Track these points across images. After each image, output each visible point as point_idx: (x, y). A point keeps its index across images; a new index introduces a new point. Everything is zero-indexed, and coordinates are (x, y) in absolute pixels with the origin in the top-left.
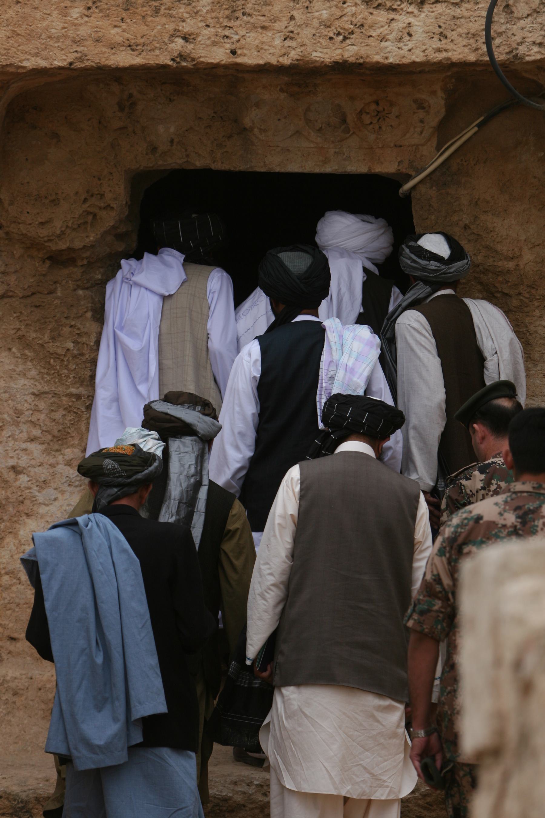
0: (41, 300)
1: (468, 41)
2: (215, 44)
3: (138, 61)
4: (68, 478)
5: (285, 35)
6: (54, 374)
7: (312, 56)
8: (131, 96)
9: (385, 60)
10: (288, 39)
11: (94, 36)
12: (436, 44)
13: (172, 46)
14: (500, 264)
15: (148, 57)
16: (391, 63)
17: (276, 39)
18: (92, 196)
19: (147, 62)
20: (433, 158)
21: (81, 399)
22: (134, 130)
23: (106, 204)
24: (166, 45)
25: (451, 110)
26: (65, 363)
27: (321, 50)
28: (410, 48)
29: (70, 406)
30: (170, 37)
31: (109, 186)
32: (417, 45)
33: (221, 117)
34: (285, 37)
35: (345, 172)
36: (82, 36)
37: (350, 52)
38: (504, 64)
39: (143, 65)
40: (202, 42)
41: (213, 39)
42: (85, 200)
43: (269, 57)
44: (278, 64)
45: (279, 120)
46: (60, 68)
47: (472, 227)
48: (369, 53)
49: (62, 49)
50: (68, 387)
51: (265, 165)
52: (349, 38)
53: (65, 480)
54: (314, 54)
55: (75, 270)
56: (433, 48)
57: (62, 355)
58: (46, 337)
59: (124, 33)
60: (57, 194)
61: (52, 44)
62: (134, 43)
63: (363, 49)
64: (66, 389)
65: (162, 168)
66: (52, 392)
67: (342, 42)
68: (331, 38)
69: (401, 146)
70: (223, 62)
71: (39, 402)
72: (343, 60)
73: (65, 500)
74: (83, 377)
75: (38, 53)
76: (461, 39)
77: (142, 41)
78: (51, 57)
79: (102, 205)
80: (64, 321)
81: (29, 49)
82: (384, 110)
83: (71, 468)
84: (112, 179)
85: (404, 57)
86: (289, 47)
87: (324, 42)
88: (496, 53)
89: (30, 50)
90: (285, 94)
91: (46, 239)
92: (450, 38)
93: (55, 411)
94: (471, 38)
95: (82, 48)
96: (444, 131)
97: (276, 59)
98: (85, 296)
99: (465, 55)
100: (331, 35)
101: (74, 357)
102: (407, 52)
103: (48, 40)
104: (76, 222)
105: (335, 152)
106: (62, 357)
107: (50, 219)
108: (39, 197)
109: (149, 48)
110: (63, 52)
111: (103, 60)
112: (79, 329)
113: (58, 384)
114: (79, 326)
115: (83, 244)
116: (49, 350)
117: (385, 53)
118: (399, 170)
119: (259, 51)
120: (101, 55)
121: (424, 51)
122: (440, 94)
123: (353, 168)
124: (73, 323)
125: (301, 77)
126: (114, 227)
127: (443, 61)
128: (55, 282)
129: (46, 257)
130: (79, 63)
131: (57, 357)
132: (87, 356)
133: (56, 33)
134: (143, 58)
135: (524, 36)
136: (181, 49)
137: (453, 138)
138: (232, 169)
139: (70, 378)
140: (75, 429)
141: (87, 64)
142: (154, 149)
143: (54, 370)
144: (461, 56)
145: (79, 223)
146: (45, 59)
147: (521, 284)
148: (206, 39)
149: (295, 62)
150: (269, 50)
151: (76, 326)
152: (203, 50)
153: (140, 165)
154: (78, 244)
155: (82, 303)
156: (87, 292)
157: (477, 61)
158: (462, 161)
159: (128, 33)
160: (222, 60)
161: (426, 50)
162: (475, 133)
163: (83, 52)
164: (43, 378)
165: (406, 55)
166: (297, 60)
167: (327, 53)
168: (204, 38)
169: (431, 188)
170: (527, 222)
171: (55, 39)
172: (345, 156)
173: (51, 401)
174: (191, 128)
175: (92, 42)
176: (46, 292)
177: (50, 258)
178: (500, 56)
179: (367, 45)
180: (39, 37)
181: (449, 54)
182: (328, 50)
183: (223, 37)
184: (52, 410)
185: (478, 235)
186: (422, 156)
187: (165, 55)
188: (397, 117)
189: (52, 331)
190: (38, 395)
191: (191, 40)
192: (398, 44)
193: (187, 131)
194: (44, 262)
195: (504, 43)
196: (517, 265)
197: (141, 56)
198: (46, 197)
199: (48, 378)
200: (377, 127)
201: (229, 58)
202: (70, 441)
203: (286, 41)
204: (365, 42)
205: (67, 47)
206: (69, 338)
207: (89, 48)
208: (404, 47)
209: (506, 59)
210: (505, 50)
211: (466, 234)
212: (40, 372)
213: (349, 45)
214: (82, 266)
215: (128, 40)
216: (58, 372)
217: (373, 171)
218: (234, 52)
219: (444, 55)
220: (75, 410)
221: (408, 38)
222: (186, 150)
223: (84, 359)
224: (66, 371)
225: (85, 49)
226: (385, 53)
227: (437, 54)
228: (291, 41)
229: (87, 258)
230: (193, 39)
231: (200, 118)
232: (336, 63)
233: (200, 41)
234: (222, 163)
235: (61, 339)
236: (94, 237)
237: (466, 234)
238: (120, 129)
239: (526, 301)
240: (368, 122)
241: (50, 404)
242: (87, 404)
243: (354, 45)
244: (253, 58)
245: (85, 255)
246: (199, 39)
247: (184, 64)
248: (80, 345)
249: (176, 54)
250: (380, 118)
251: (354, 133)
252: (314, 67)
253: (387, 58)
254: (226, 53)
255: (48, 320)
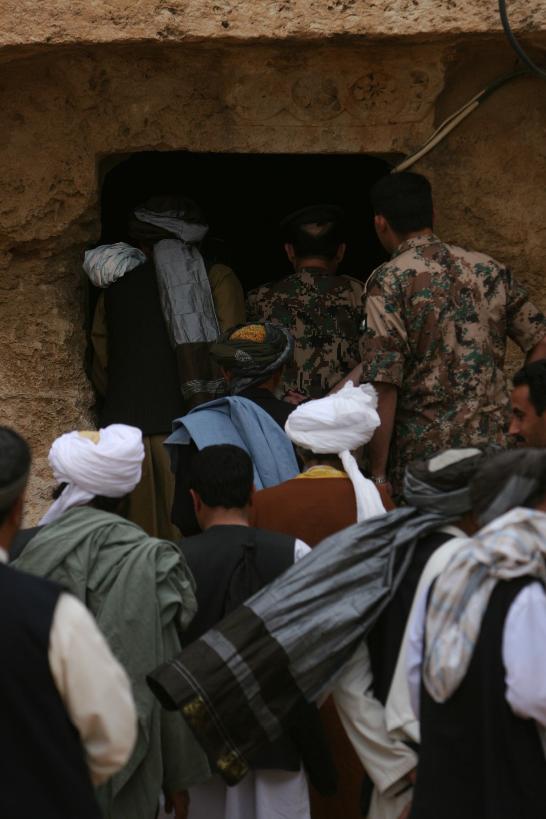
0: (3, 296)
1: (479, 9)
2: (205, 15)
3: (122, 35)
4: (39, 490)
5: (280, 5)
6: (21, 376)
7: (311, 27)
8: (103, 73)
9: (390, 31)
10: (284, 10)
11: (73, 9)
12: (444, 12)
13: (158, 18)
14: (504, 249)
15: (132, 31)
16: (396, 34)
17: (271, 10)
18: (60, 182)
19: (132, 37)
20: (431, 136)
21: (52, 403)
22: (105, 110)
23: (76, 191)
24: (152, 18)
25: (451, 82)
26: (33, 365)
27: (319, 21)
28: (416, 17)
29: (40, 411)
30: (155, 9)
31: (78, 171)
32: (424, 14)
33: (201, 95)
34: (281, 7)
35: (335, 152)
36: (60, 9)
37: (352, 22)
38: (517, 34)
39: (127, 40)
40: (190, 14)
41: (203, 10)
42: (52, 187)
43: (264, 29)
44: (274, 36)
45: (264, 97)
46: (37, 44)
47: (473, 210)
48: (372, 23)
49: (39, 24)
50: (37, 390)
51: (248, 146)
52: (350, 8)
53: (36, 492)
54: (313, 25)
55: (38, 263)
56: (441, 18)
57: (29, 356)
58: (12, 336)
59: (106, 5)
60: (21, 180)
61: (28, 18)
62: (117, 16)
63: (365, 19)
64: (35, 393)
65: (134, 151)
66: (20, 397)
67: (342, 12)
68: (330, 8)
69: (395, 123)
70: (214, 36)
71: (6, 407)
72: (344, 32)
73: (37, 513)
74: (52, 379)
75: (13, 28)
76: (471, 7)
77: (126, 13)
78: (27, 33)
79: (71, 191)
80: (29, 318)
81: (3, 23)
82: (378, 84)
83: (43, 479)
84: (82, 164)
85: (409, 27)
86: (285, 18)
87: (323, 12)
88: (509, 22)
89: (4, 25)
90: (273, 69)
91: (10, 230)
92: (459, 6)
93: (24, 417)
94: (482, 5)
95: (61, 22)
96: (441, 108)
97: (271, 31)
98: (48, 291)
99: (476, 24)
100: (331, 4)
101: (43, 358)
102: (412, 22)
103: (24, 13)
104: (42, 211)
105: (324, 131)
106: (30, 358)
107: (15, 207)
108: (3, 184)
109: (133, 21)
110: (40, 26)
111: (84, 34)
112: (46, 327)
113: (26, 387)
114: (46, 324)
115: (49, 235)
116: (15, 350)
117: (389, 24)
118: (394, 149)
119: (253, 23)
120: (82, 29)
121: (431, 21)
122: (441, 66)
123: (344, 148)
124: (39, 321)
125: (294, 50)
126: (82, 216)
127: (452, 31)
128: (18, 277)
129: (8, 249)
130: (58, 39)
131: (24, 358)
132: (56, 357)
133: (32, 6)
134: (128, 33)
135: (539, 3)
136: (168, 21)
137: (452, 114)
138: (213, 151)
139: (39, 381)
140: (46, 436)
141: (66, 39)
142: (127, 130)
143: (21, 372)
144: (471, 26)
145: (45, 211)
146: (21, 35)
147: (527, 271)
148: (195, 11)
149: (292, 34)
150: (263, 21)
151: (42, 324)
152: (192, 22)
153: (112, 148)
154: (44, 235)
155: (46, 299)
156: (51, 287)
157: (488, 30)
158: (461, 138)
159: (110, 5)
160: (214, 34)
161: (433, 19)
162: (476, 108)
163: (61, 26)
164: (9, 382)
165: (412, 25)
166: (294, 32)
167: (326, 24)
168: (193, 10)
169: (427, 168)
170: (533, 204)
171: (30, 12)
172: (335, 135)
173: (18, 406)
174: (168, 107)
175: (71, 15)
176: (8, 288)
177: (12, 250)
178: (515, 25)
179: (370, 15)
180: (13, 11)
181: (459, 24)
182: (327, 20)
183: (214, 8)
184: (21, 416)
185: (480, 218)
186: (418, 133)
187: (151, 29)
188: (392, 92)
189: (17, 329)
190: (5, 400)
191: (179, 12)
192: (403, 13)
193: (163, 110)
194: (6, 254)
195: (518, 10)
196: (522, 251)
197: (125, 30)
198: (10, 184)
199: (15, 381)
200: (370, 103)
201: (221, 31)
202: (41, 450)
203: (281, 12)
204: (367, 12)
205: (45, 21)
206: (35, 337)
207: (68, 22)
208: (410, 17)
209: (520, 28)
210: (518, 18)
211: (467, 218)
212: (6, 375)
213: (350, 15)
214: (45, 258)
215: (110, 13)
216: (26, 374)
217: (365, 151)
218: (225, 25)
219: (453, 24)
220: (45, 416)
221: (413, 7)
222: (161, 131)
223: (53, 359)
224: (34, 373)
225: (64, 23)
226: (389, 24)
227: (445, 24)
228: (287, 12)
229: (51, 250)
230: (181, 10)
231: (178, 96)
232: (336, 35)
233: (189, 13)
234: (201, 144)
235: (27, 338)
236: (61, 227)
237: (467, 218)
238: (90, 109)
239: (533, 289)
240: (361, 98)
241: (17, 410)
242: (59, 409)
243: (355, 15)
244: (247, 30)
245: (50, 247)
246: (188, 10)
247: (172, 38)
248: (48, 345)
249: (163, 27)
250: (373, 93)
251: (345, 110)
252: (312, 39)
253: (391, 29)
254: (217, 26)
255: (12, 318)
